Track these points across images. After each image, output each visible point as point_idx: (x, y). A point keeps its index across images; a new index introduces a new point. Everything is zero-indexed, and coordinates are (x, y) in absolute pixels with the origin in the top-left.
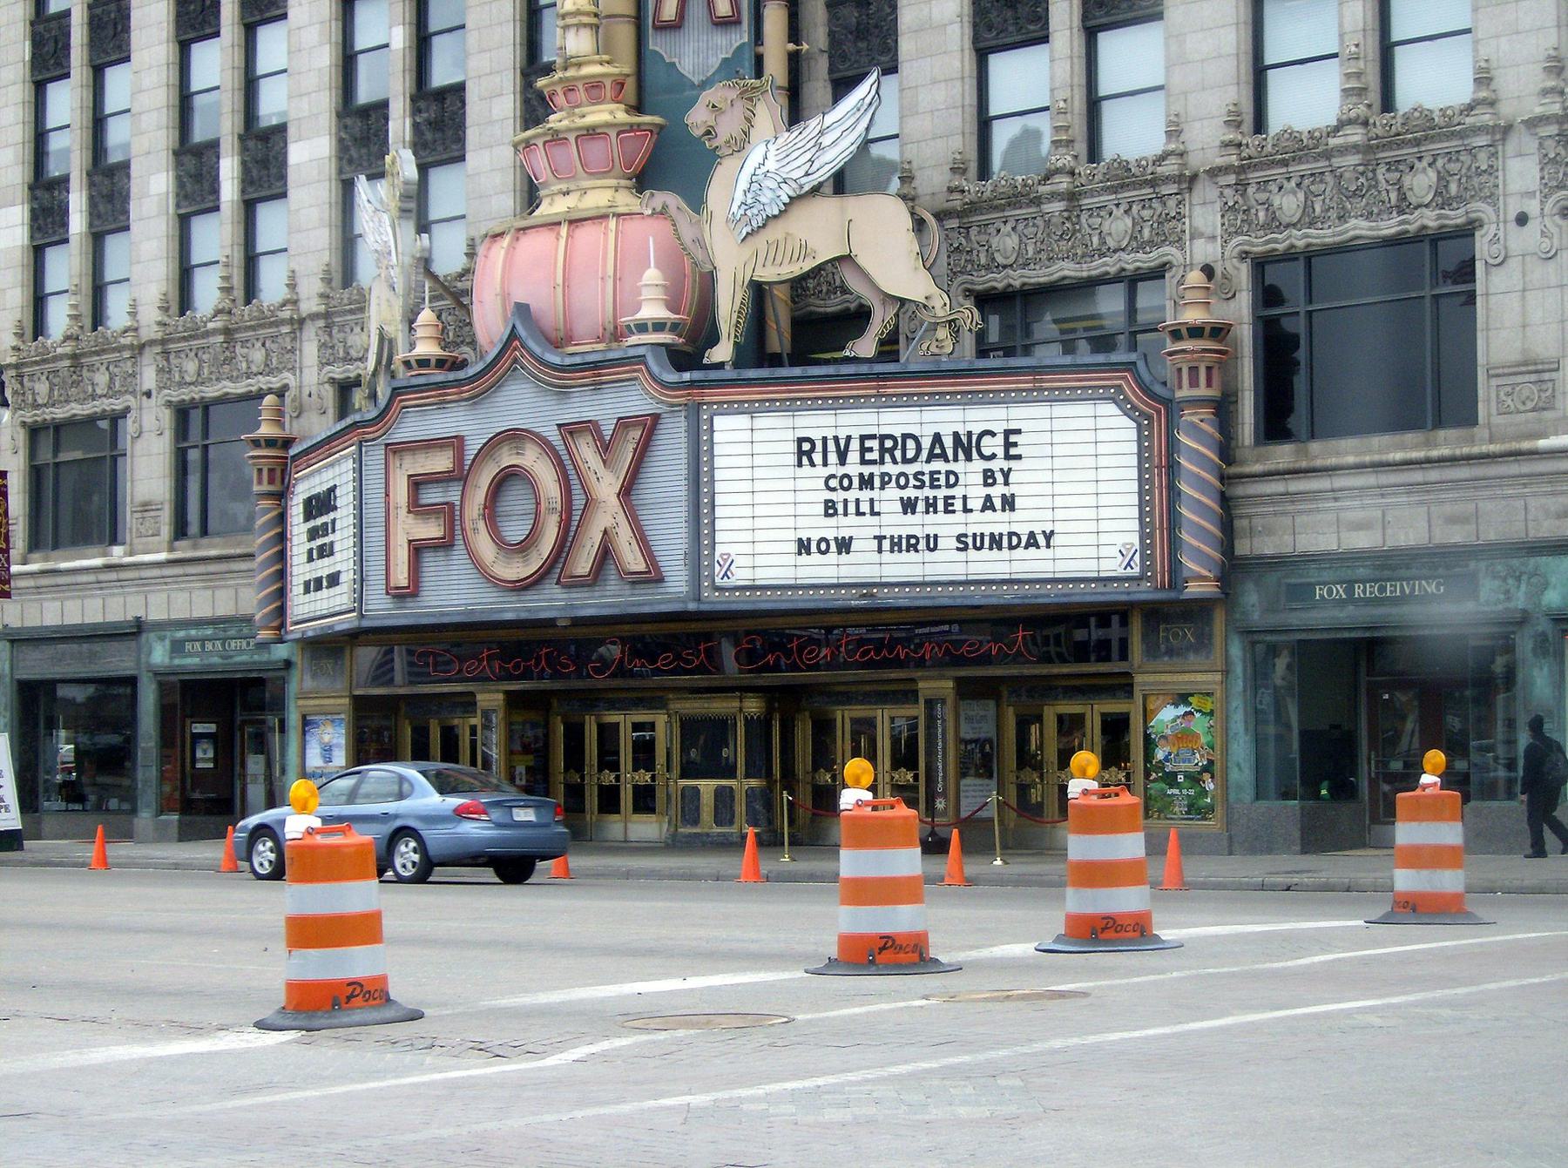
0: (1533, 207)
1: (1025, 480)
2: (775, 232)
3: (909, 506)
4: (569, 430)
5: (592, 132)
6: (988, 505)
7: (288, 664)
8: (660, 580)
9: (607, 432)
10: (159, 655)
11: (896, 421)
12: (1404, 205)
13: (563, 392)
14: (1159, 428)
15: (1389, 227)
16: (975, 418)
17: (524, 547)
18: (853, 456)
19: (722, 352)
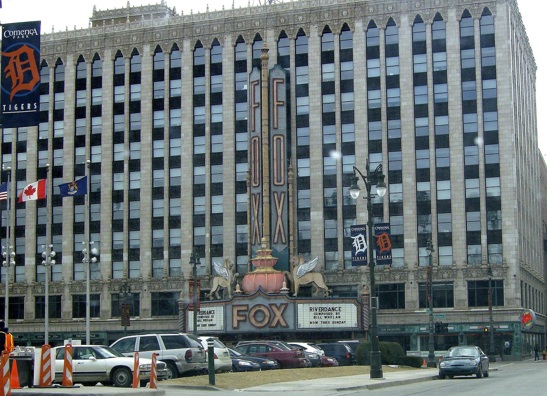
0: (413, 281)
1: (342, 314)
2: (303, 278)
3: (326, 317)
4: (271, 305)
5: (269, 260)
6: (337, 317)
8: (288, 327)
9: (278, 305)
11: (324, 305)
12: (395, 280)
13: (269, 299)
14: (360, 307)
15: (392, 282)
16: (335, 305)
17: (261, 322)
18: (318, 310)
19: (295, 294)
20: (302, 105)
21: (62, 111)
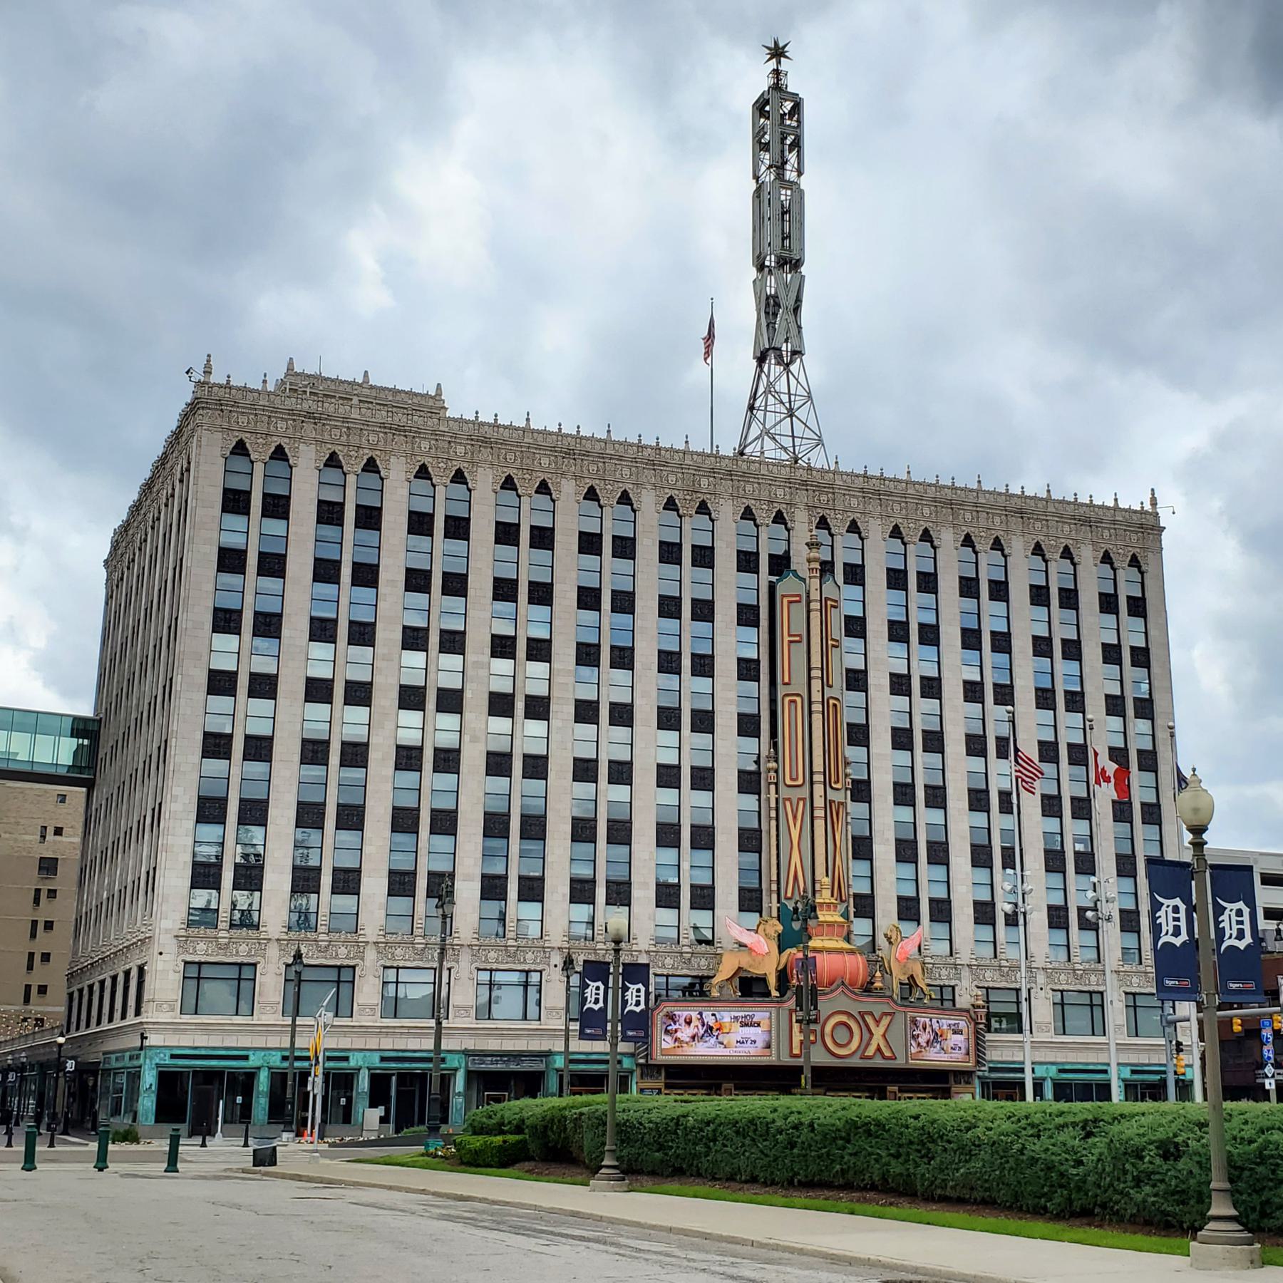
7: (632, 1072)
10: (559, 1062)
12: (486, 961)
20: (749, 643)
21: (965, 646)
